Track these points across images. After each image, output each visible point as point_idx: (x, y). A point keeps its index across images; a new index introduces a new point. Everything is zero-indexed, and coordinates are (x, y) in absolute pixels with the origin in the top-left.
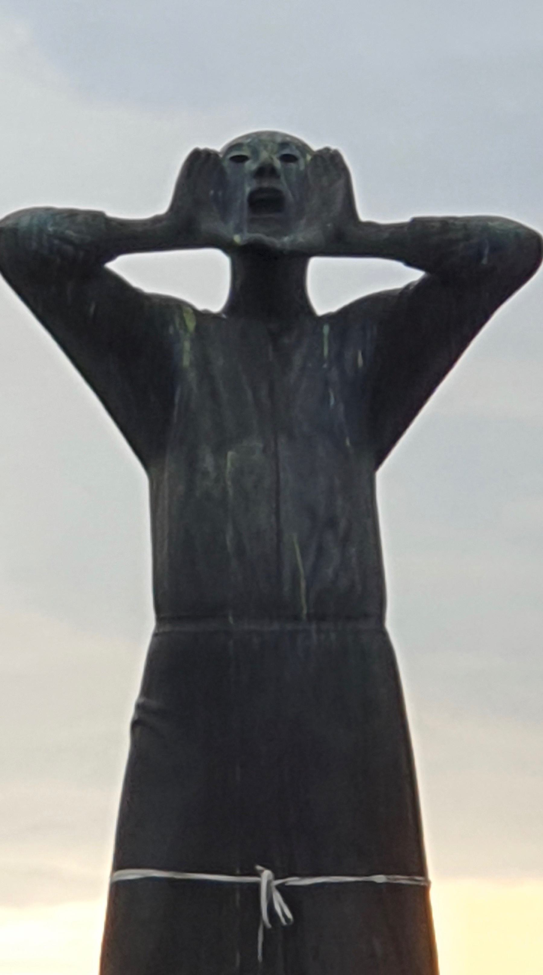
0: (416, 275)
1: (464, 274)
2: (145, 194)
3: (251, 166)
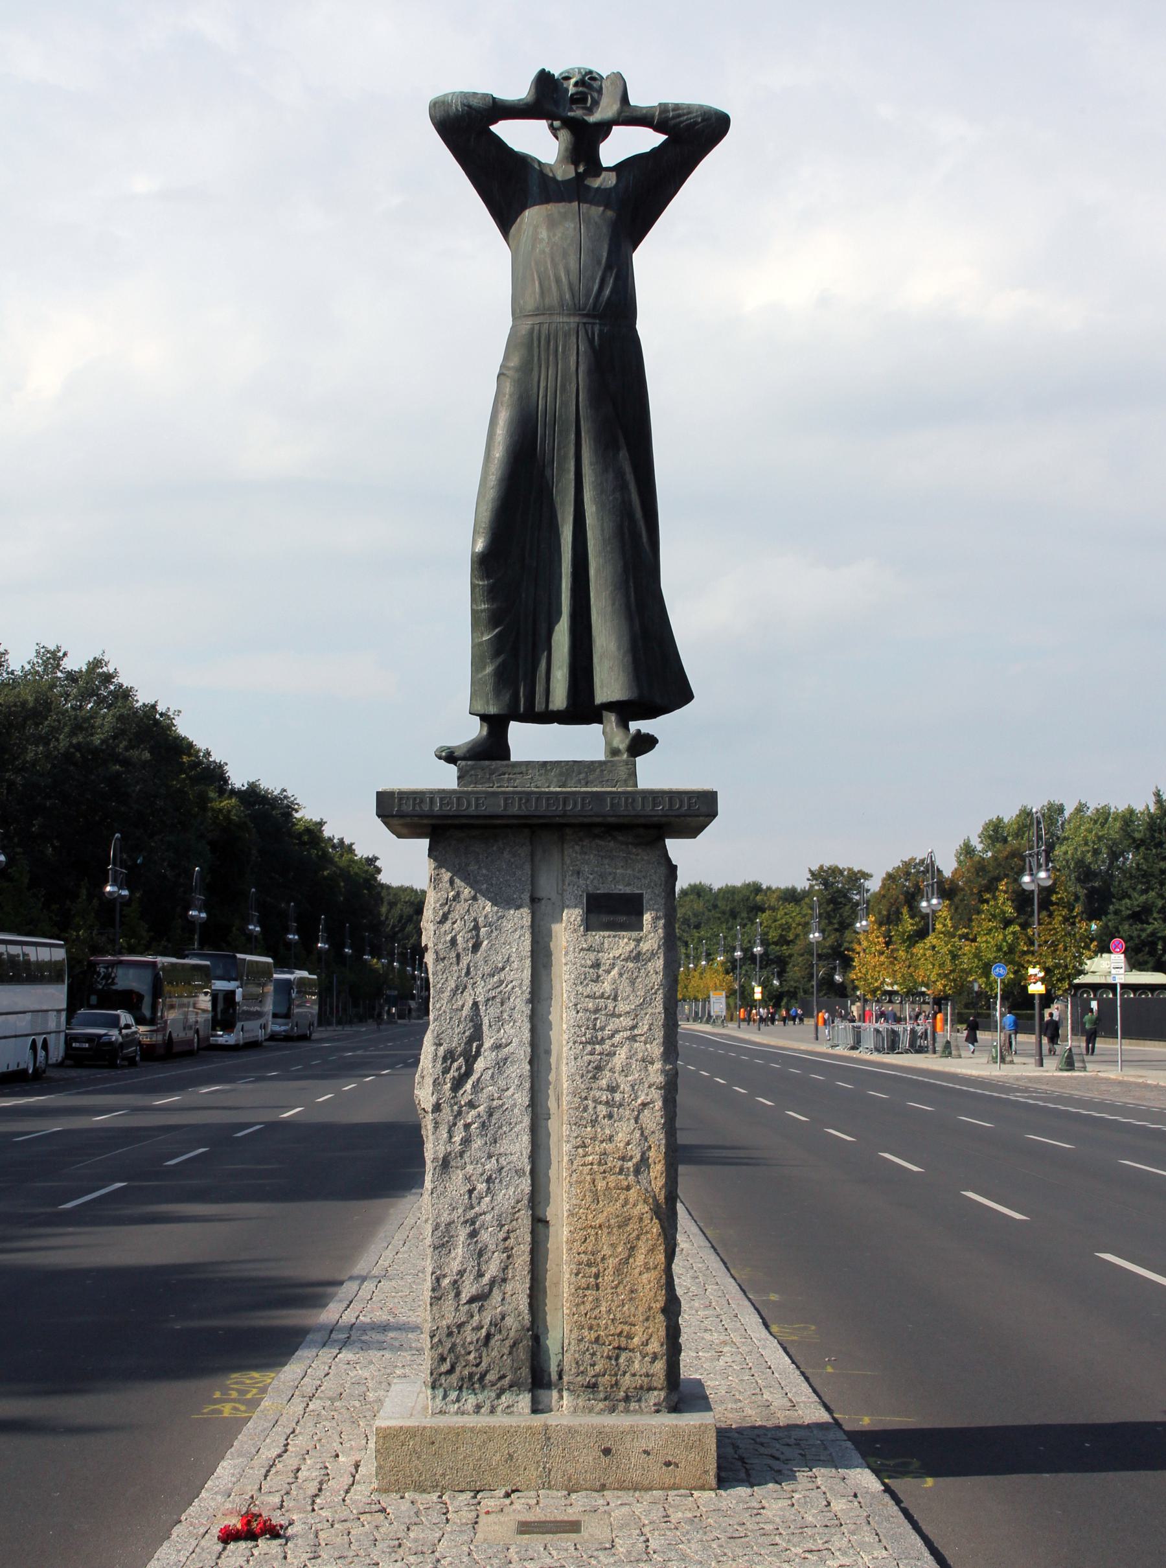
0: (662, 138)
1: (692, 135)
2: (518, 90)
3: (573, 81)
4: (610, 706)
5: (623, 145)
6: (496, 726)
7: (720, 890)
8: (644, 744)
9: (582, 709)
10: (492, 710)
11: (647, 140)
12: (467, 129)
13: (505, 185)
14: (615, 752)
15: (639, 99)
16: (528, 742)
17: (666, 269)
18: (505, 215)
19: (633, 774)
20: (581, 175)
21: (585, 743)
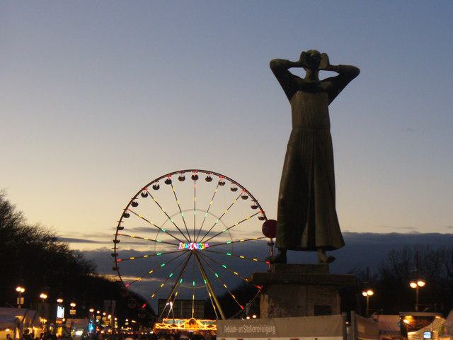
1: (347, 74)
2: (296, 58)
4: (320, 247)
5: (323, 75)
6: (283, 251)
7: (446, 337)
8: (331, 259)
9: (311, 247)
10: (283, 247)
11: (334, 74)
12: (280, 69)
13: (290, 85)
14: (322, 261)
15: (333, 62)
16: (293, 257)
17: (340, 112)
18: (290, 95)
19: (328, 269)
20: (311, 88)
21: (311, 258)
